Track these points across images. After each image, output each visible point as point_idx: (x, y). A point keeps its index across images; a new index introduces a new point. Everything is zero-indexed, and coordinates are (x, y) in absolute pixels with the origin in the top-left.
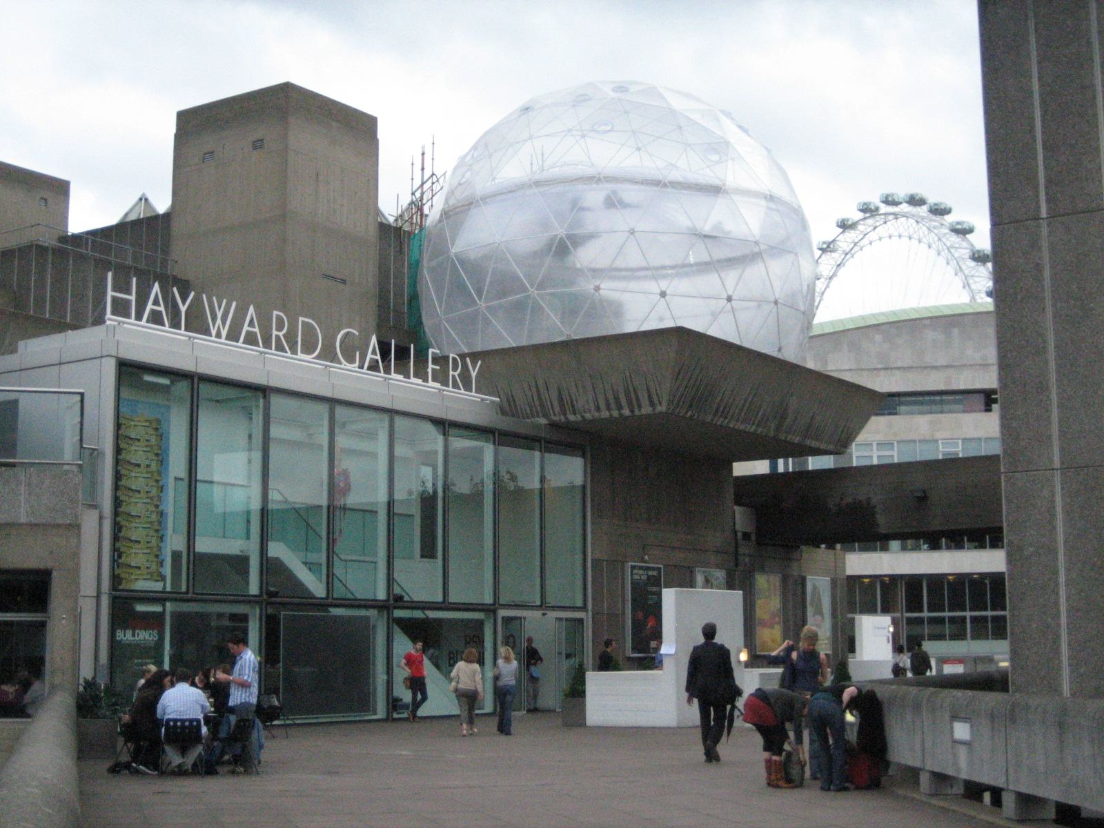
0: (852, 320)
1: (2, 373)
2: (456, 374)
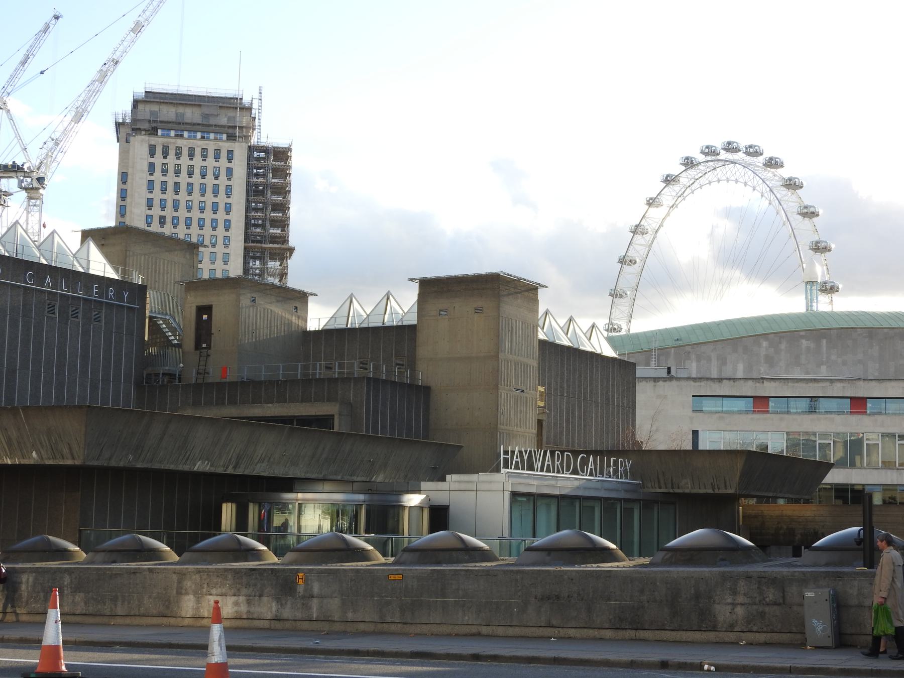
0: (742, 323)
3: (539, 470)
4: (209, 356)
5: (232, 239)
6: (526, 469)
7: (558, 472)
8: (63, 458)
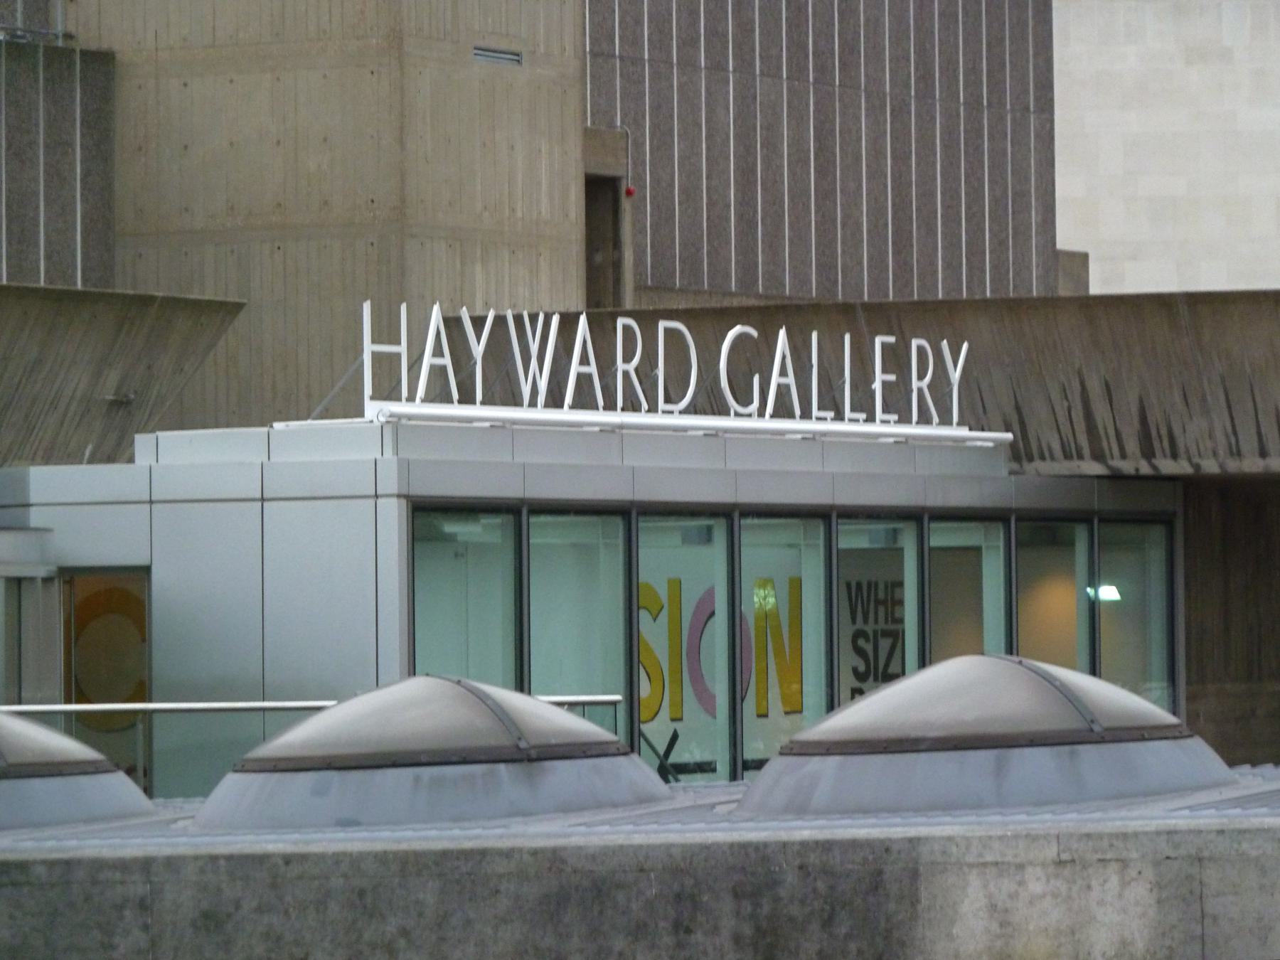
1: (1203, 956)
3: (541, 399)
6: (479, 396)
7: (632, 405)
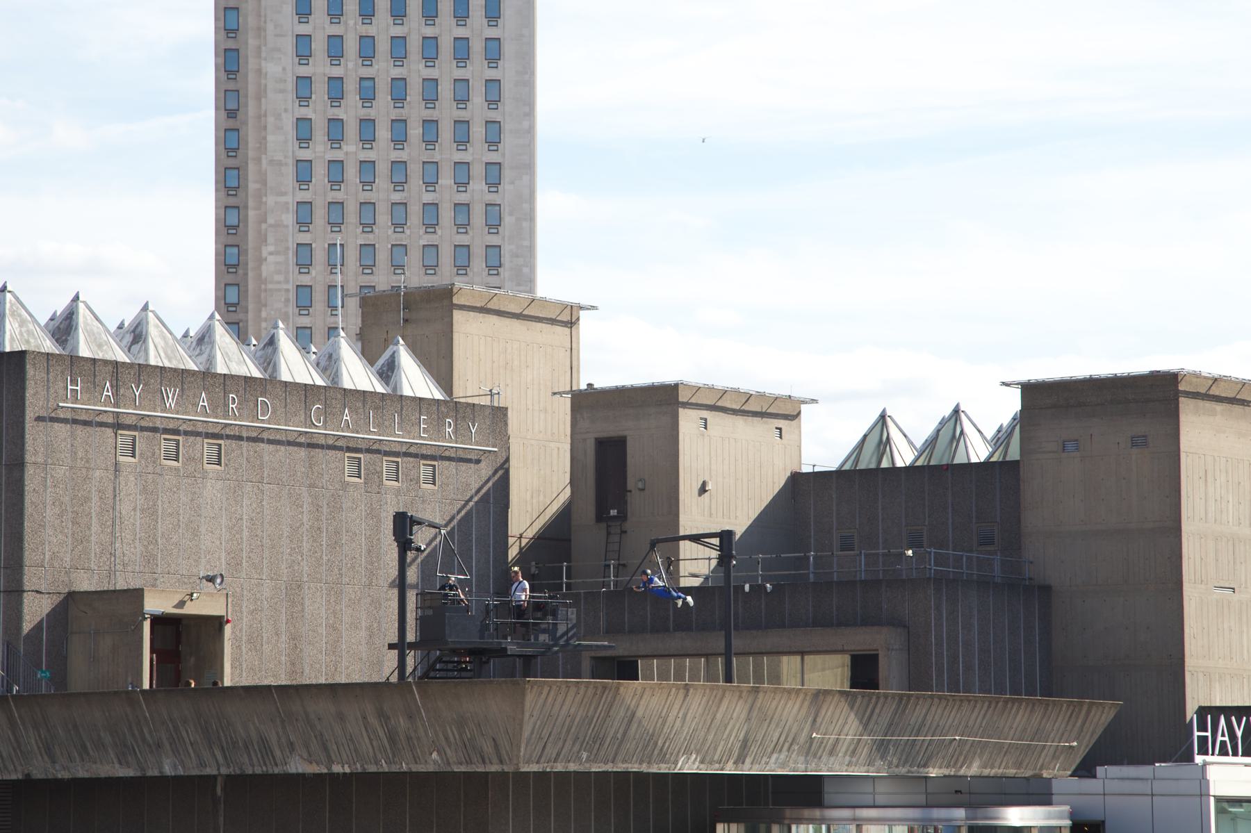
2: (450, 430)
4: (625, 532)
5: (507, 127)
6: (1240, 753)
8: (484, 762)
